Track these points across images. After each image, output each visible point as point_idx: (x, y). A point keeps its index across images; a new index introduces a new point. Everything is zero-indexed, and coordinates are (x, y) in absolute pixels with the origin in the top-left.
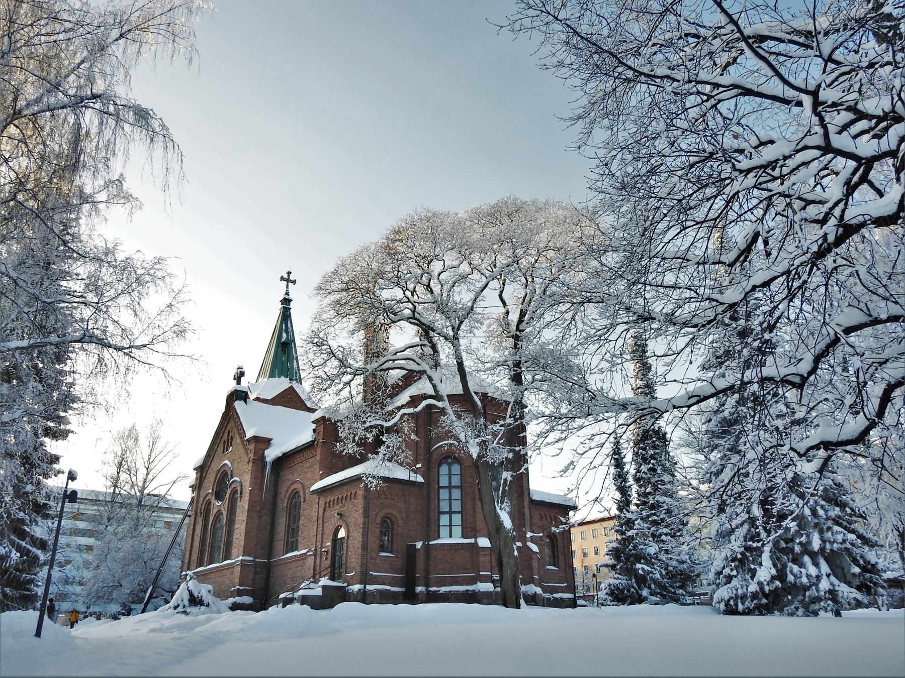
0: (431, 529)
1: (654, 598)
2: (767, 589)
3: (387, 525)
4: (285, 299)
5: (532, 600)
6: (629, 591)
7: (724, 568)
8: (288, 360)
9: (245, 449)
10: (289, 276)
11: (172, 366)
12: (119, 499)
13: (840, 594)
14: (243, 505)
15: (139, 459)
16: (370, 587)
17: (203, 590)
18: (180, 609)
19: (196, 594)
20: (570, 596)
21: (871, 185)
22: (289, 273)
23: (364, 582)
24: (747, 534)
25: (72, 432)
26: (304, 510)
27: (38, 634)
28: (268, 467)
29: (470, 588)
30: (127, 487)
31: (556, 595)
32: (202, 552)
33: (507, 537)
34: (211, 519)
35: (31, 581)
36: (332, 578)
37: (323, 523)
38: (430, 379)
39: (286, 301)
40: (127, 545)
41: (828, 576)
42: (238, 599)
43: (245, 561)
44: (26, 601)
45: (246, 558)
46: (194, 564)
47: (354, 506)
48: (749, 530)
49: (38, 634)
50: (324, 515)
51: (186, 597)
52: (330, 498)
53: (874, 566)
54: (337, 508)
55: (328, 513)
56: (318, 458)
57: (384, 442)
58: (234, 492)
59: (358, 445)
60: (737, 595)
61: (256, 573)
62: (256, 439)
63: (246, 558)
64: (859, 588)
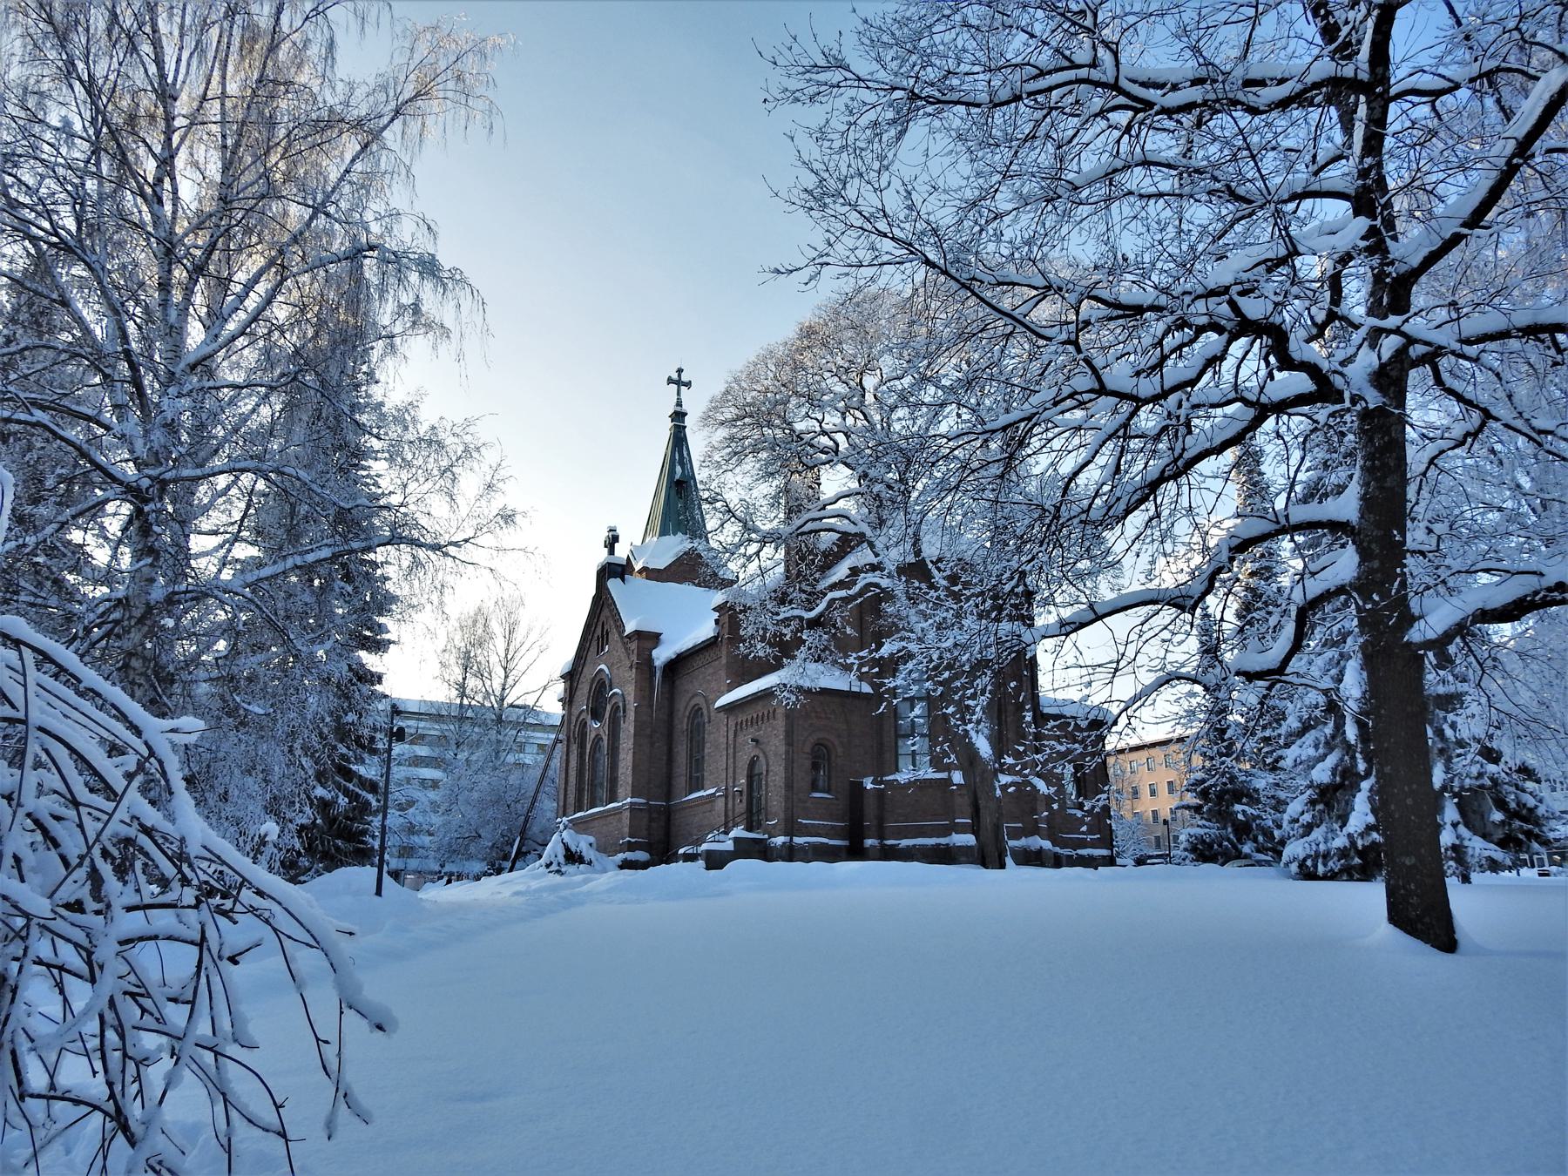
0: (885, 760)
1: (1261, 857)
2: (1360, 843)
3: (820, 757)
4: (676, 413)
5: (1030, 858)
6: (1220, 845)
7: (1303, 813)
8: (686, 508)
9: (626, 649)
10: (679, 376)
11: (503, 564)
12: (470, 714)
13: (1470, 851)
14: (628, 728)
15: (493, 656)
16: (798, 840)
17: (583, 843)
18: (554, 867)
19: (573, 849)
20: (1105, 852)
21: (192, 943)
22: (680, 371)
23: (790, 833)
24: (1337, 766)
25: (394, 642)
26: (709, 734)
27: (379, 892)
28: (658, 674)
29: (943, 841)
30: (479, 698)
31: (1080, 852)
32: (580, 791)
33: (984, 771)
34: (588, 746)
35: (364, 832)
36: (749, 829)
37: (735, 753)
38: (872, 545)
39: (679, 416)
40: (484, 780)
41: (1455, 825)
42: (629, 855)
43: (635, 804)
44: (362, 856)
45: (635, 800)
46: (571, 809)
47: (774, 729)
48: (1342, 760)
49: (379, 892)
50: (735, 741)
51: (561, 852)
52: (742, 717)
53: (1532, 810)
54: (751, 732)
55: (740, 739)
56: (724, 661)
57: (805, 641)
58: (616, 709)
59: (771, 645)
60: (1317, 854)
61: (651, 820)
62: (638, 635)
63: (635, 800)
64: (1502, 844)
